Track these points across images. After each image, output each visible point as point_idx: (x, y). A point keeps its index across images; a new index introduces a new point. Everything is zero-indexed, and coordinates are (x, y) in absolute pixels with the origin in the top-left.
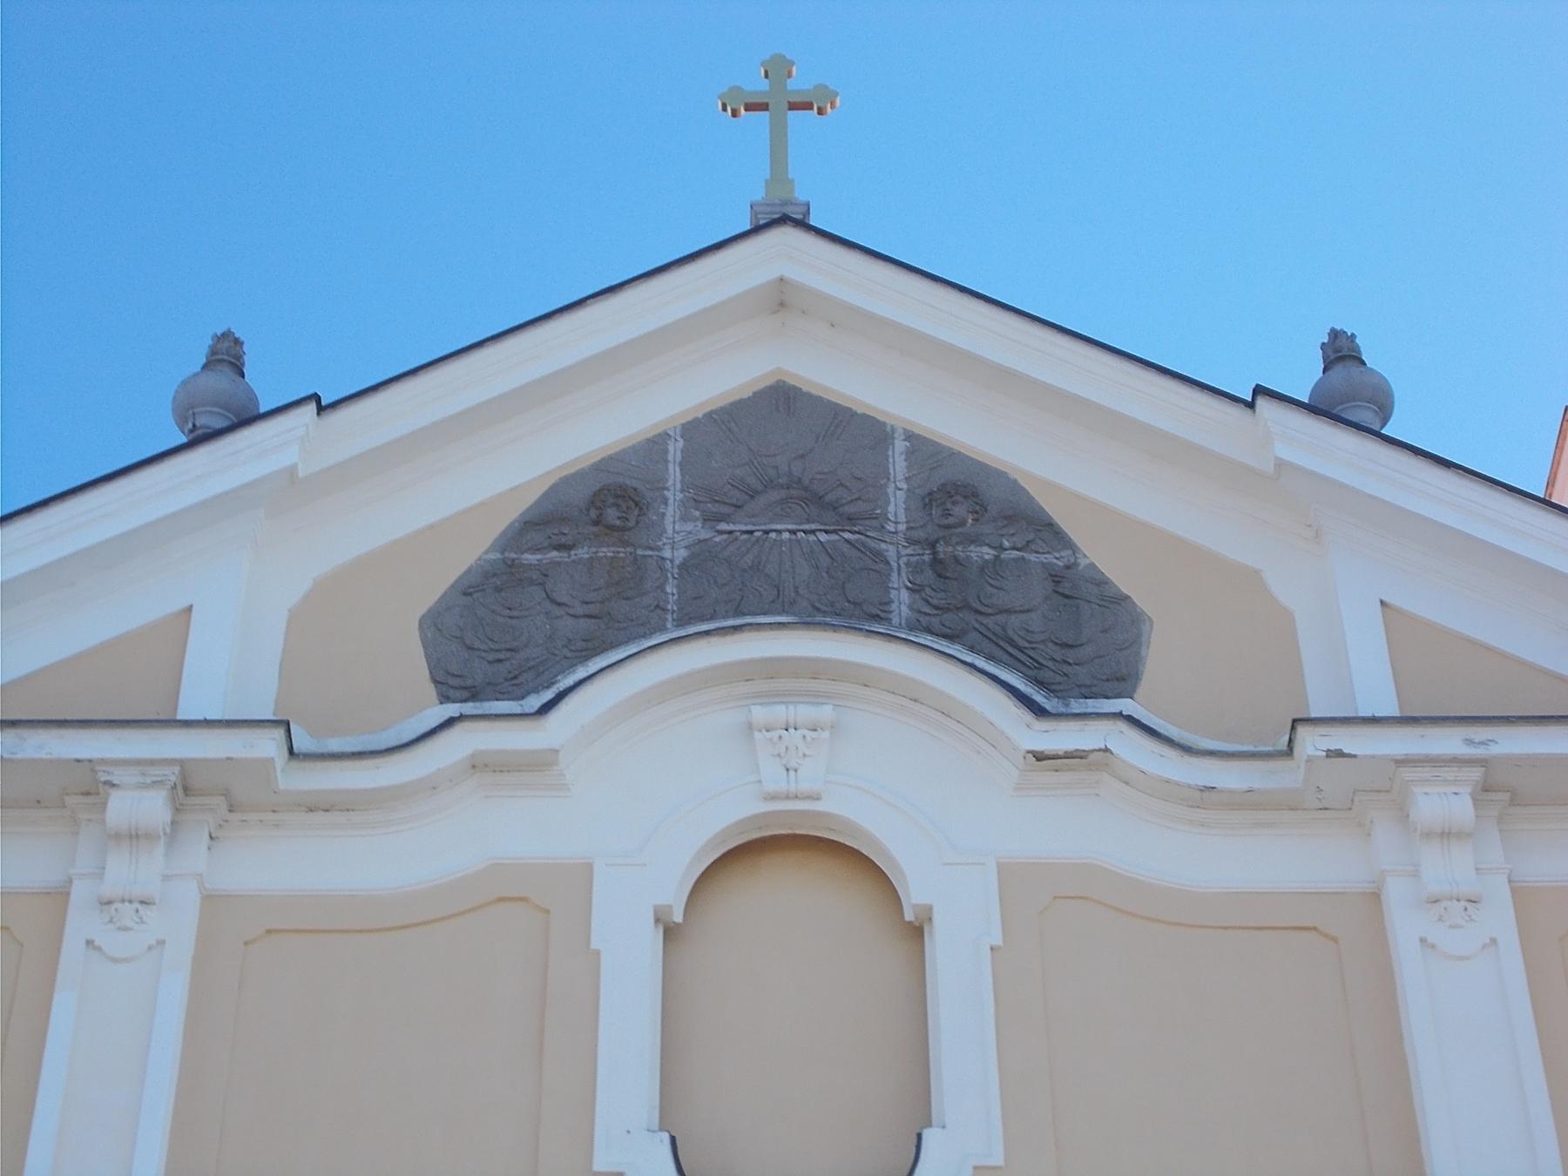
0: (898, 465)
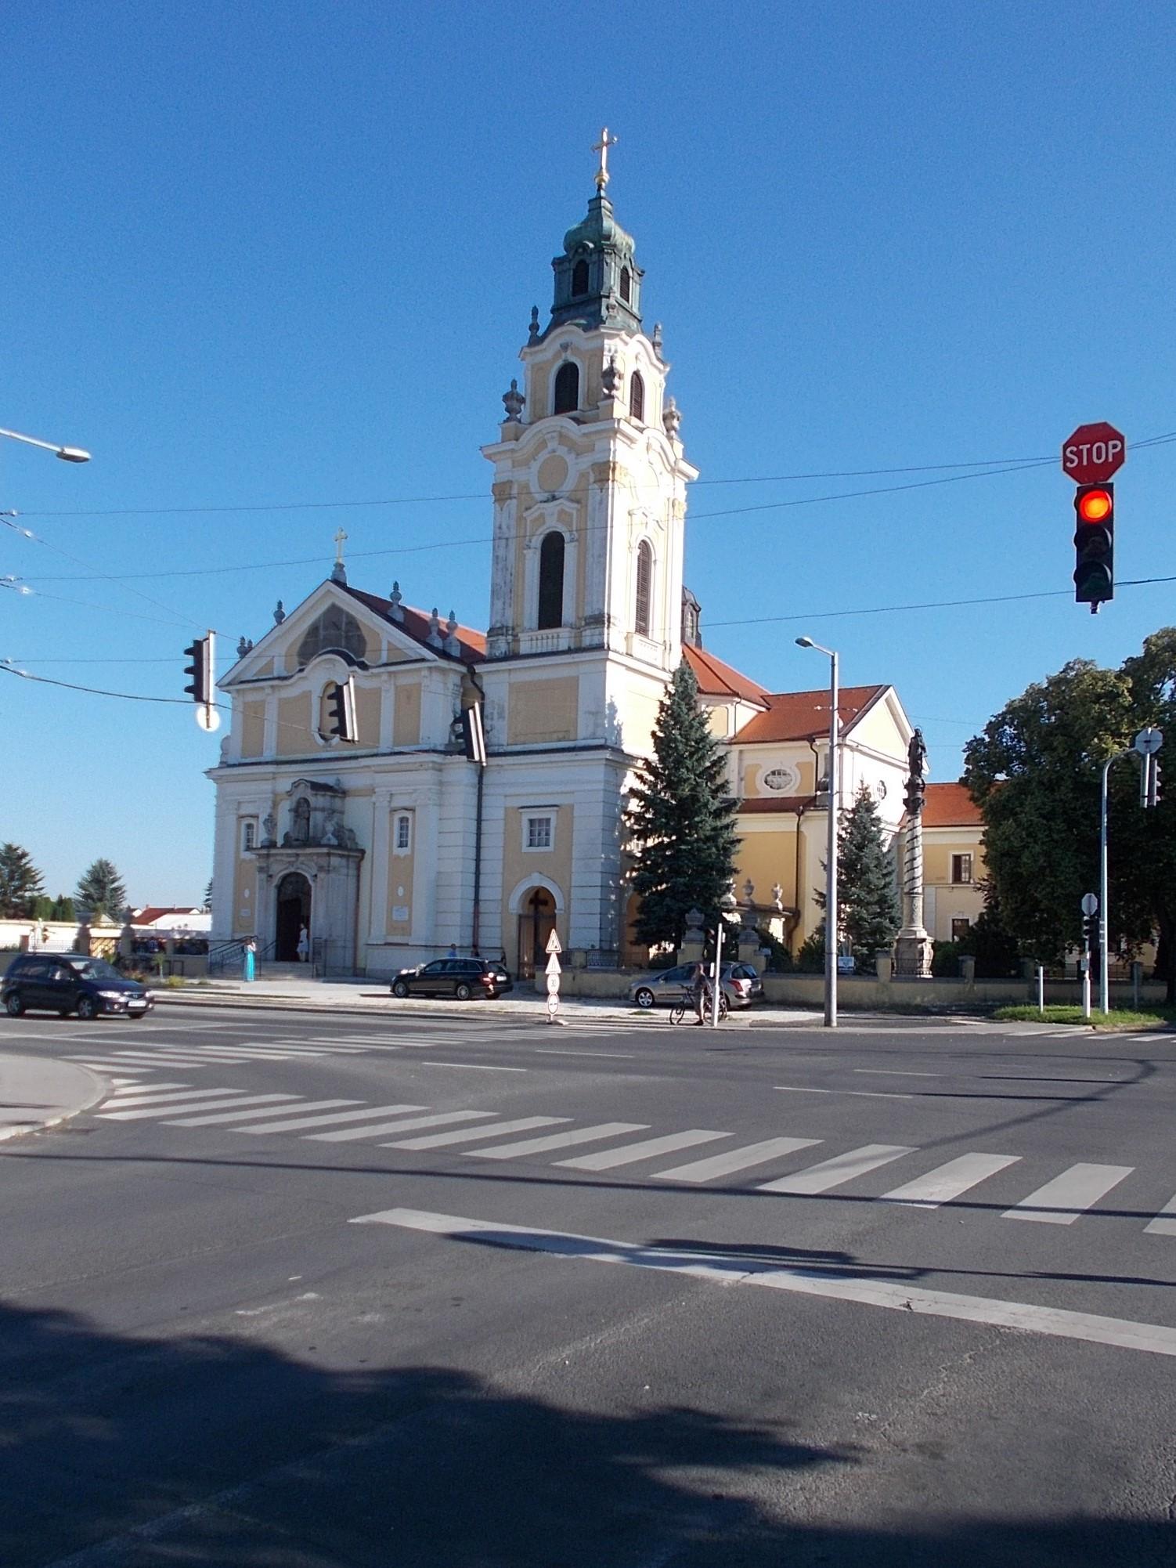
0: (344, 620)
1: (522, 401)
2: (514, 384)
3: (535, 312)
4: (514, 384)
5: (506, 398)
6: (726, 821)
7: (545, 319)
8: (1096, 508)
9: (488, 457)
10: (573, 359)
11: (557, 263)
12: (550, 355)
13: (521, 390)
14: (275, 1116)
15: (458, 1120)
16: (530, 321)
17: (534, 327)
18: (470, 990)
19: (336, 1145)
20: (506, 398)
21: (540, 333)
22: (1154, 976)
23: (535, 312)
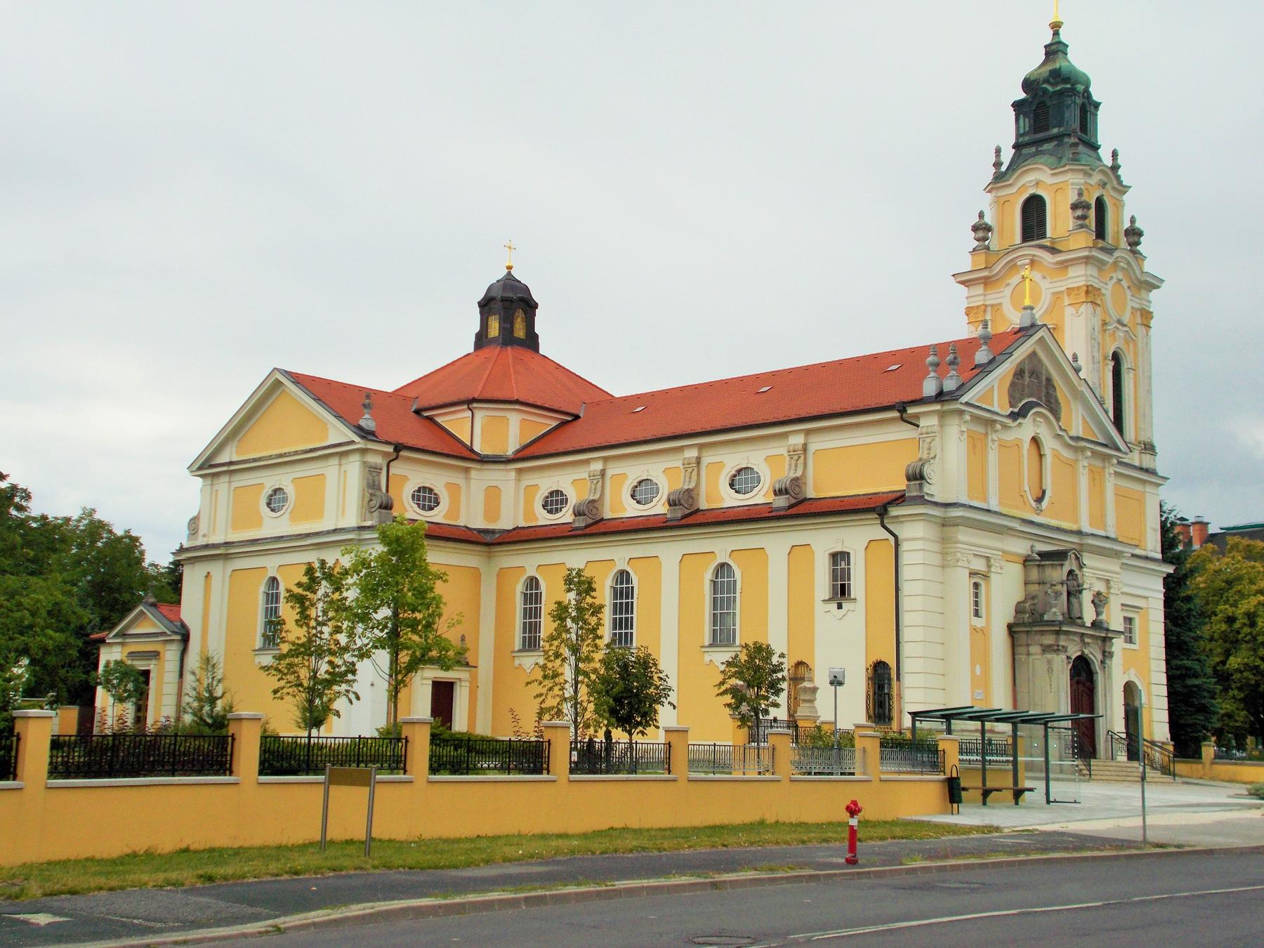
1: (988, 229)
2: (981, 215)
3: (998, 151)
4: (981, 215)
5: (975, 228)
6: (300, 591)
7: (1007, 155)
8: (962, 868)
9: (962, 283)
10: (1040, 192)
11: (1017, 106)
12: (1019, 191)
13: (988, 219)
14: (470, 699)
15: (1191, 823)
16: (993, 160)
17: (997, 164)
18: (29, 654)
19: (436, 896)
20: (975, 228)
21: (1003, 168)
22: (509, 273)
23: (998, 151)
